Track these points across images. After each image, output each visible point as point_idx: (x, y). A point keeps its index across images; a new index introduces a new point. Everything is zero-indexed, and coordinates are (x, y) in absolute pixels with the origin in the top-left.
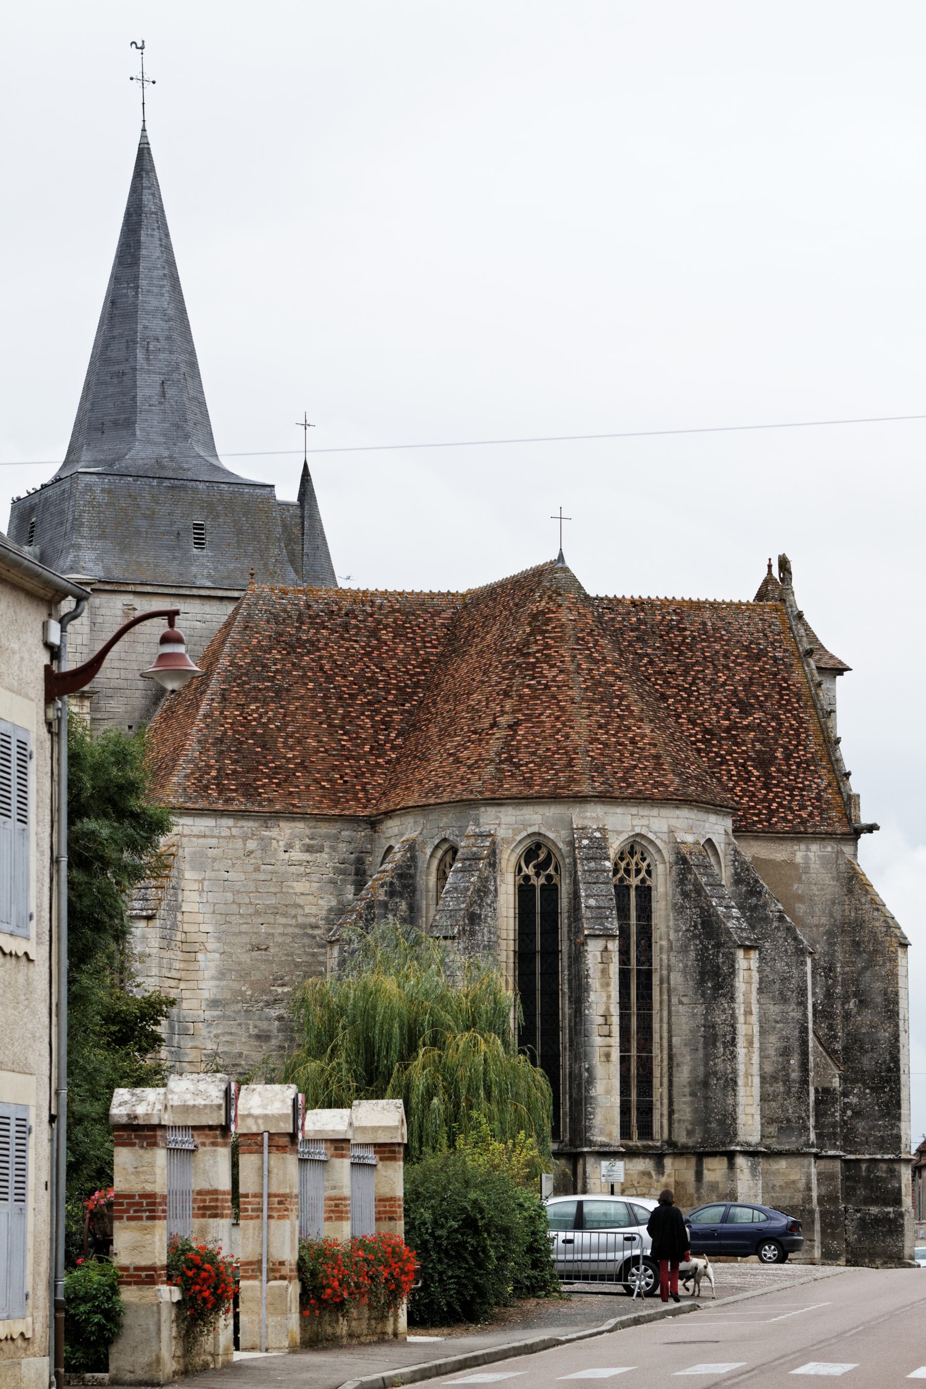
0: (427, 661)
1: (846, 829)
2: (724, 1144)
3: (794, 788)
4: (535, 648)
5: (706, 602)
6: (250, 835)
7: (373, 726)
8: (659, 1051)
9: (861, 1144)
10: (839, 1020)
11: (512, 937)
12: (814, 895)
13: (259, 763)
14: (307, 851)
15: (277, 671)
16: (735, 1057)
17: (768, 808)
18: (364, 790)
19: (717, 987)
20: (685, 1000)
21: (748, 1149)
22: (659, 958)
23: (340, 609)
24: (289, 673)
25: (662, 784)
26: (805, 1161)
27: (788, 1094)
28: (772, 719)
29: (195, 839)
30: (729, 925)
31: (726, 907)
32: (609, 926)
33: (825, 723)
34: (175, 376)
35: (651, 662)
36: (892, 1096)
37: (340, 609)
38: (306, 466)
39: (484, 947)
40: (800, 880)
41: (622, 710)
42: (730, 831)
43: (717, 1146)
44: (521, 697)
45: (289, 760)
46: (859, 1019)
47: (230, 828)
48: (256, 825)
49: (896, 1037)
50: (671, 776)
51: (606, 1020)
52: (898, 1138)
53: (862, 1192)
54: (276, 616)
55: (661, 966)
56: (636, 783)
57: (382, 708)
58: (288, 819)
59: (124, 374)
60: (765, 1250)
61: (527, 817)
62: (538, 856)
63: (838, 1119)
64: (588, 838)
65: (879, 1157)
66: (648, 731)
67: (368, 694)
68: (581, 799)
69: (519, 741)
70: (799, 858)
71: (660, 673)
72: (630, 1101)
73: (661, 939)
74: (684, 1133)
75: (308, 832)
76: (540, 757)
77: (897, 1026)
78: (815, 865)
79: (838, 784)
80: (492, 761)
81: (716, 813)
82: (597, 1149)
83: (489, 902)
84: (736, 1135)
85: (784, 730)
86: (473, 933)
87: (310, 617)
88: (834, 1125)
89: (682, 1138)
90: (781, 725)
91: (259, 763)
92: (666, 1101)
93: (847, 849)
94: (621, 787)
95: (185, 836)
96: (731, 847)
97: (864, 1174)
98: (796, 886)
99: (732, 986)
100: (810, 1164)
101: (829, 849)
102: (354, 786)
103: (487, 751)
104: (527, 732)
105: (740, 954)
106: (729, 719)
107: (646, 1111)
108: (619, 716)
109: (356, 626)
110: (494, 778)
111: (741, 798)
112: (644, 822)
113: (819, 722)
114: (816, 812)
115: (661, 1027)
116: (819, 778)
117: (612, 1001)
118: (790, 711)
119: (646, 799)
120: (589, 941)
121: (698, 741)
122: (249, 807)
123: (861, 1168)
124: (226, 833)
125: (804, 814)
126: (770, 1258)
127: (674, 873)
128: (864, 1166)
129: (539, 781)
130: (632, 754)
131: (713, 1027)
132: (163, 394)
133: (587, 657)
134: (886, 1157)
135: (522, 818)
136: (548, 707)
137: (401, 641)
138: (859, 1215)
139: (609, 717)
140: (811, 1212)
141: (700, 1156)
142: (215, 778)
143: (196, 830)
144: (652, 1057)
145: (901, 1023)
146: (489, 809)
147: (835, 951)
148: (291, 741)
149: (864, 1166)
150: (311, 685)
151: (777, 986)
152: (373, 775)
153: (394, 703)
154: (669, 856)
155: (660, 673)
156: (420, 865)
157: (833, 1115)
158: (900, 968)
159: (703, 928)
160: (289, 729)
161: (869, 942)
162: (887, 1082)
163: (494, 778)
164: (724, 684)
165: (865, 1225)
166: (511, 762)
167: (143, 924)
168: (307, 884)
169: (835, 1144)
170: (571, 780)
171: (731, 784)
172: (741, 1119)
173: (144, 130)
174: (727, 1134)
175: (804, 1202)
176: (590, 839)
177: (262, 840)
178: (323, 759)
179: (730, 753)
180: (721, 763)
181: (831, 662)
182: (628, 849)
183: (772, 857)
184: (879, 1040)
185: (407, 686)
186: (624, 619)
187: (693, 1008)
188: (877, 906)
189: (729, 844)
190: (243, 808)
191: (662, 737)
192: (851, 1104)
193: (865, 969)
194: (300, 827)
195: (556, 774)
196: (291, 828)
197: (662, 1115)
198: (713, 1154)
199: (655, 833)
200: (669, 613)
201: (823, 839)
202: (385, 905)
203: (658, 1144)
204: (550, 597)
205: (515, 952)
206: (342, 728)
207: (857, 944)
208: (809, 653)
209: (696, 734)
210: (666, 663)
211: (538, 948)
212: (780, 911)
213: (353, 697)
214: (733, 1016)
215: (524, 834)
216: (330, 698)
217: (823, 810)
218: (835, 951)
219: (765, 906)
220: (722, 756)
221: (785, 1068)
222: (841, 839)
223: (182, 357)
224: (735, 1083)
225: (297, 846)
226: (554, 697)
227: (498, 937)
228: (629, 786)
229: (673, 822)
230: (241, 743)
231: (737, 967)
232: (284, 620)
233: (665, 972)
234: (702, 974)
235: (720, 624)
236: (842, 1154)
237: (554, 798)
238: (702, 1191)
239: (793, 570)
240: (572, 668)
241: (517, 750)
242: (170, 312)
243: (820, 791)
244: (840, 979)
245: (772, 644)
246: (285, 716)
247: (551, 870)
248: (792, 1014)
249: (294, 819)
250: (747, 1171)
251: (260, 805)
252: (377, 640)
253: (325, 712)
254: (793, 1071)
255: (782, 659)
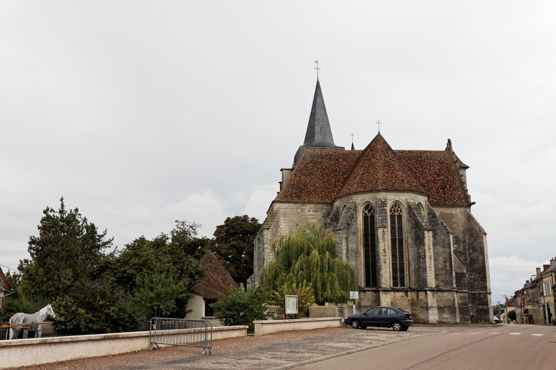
0: (351, 166)
1: (467, 204)
2: (424, 288)
3: (452, 194)
4: (370, 155)
5: (428, 151)
6: (298, 208)
7: (335, 181)
8: (405, 261)
9: (476, 289)
10: (468, 255)
11: (362, 230)
12: (459, 222)
13: (302, 190)
14: (314, 212)
15: (310, 169)
16: (426, 262)
17: (444, 199)
18: (331, 196)
19: (420, 242)
20: (412, 246)
21: (431, 289)
22: (405, 235)
23: (329, 154)
24: (314, 169)
25: (404, 187)
26: (452, 293)
27: (446, 274)
28: (446, 178)
29: (283, 209)
30: (423, 224)
31: (422, 219)
32: (385, 224)
33: (461, 178)
34: (323, 126)
35: (412, 165)
36: (484, 275)
37: (329, 154)
38: (353, 144)
39: (353, 233)
40: (454, 218)
41: (393, 168)
42: (427, 201)
43: (422, 288)
44: (365, 167)
45: (311, 189)
46: (473, 254)
47: (293, 206)
48: (300, 205)
49: (484, 259)
50: (407, 185)
51: (384, 251)
52: (486, 287)
53: (477, 302)
54: (312, 156)
55: (405, 237)
56: (396, 186)
57: (338, 177)
58: (309, 204)
59: (313, 127)
60: (395, 326)
61: (365, 197)
62: (369, 208)
63: (466, 281)
64: (381, 201)
65: (481, 292)
66: (400, 174)
67: (334, 174)
68: (379, 191)
69: (364, 178)
70: (454, 212)
71: (415, 167)
72: (397, 276)
73: (405, 230)
74: (413, 285)
75: (314, 207)
76: (369, 181)
77: (484, 256)
78: (459, 214)
79: (465, 193)
80: (356, 183)
81: (422, 195)
82: (383, 289)
83: (354, 220)
84: (427, 285)
85: (449, 180)
86: (348, 229)
87: (321, 156)
88: (465, 283)
89: (413, 286)
90: (448, 179)
91: (302, 190)
92: (408, 276)
93: (468, 210)
94: (391, 188)
95: (281, 208)
96: (427, 205)
97: (477, 297)
98: (453, 219)
99: (424, 241)
100: (454, 294)
101: (462, 210)
102: (328, 195)
103: (355, 181)
104: (366, 175)
105: (426, 232)
106: (434, 178)
107: (402, 278)
108: (392, 170)
109: (333, 158)
110: (356, 187)
111: (437, 197)
112: (399, 197)
113: (459, 178)
114: (458, 200)
115: (406, 254)
116: (459, 192)
117: (386, 246)
118: (451, 176)
119: (398, 190)
120: (379, 229)
121: (425, 183)
122: (298, 201)
123: (476, 295)
124: (292, 207)
125: (455, 201)
126: (397, 329)
127: (408, 211)
128: (477, 295)
129: (368, 187)
130: (395, 179)
131: (420, 254)
132: (321, 130)
133: (384, 156)
134: (483, 292)
135: (363, 197)
136: (372, 169)
137: (345, 161)
138: (476, 308)
139: (389, 170)
140: (455, 308)
141: (418, 291)
142: (290, 194)
143: (283, 207)
144: (404, 263)
145: (485, 255)
146: (355, 195)
147: (465, 236)
148: (312, 185)
149: (477, 295)
150: (319, 172)
151: (442, 243)
152: (333, 193)
153: (341, 176)
154: (406, 206)
155: (415, 167)
156: (340, 213)
157: (465, 280)
158: (484, 240)
159: (416, 225)
160: (312, 182)
161: (475, 233)
162: (482, 271)
163: (356, 187)
164: (433, 170)
165: (478, 311)
166: (361, 183)
167: (266, 230)
168: (315, 220)
169: (466, 288)
170: (377, 186)
171: (434, 194)
172: (428, 280)
173: (318, 78)
174: (424, 285)
175: (453, 305)
176: (381, 201)
177: (302, 209)
178: (320, 189)
179: (434, 186)
180: (431, 189)
181: (464, 166)
182: (394, 204)
183: (446, 212)
184: (479, 260)
185: (345, 171)
186: (405, 155)
187: (414, 249)
188: (477, 224)
189: (426, 204)
190: (296, 201)
191: (404, 175)
192: (472, 278)
193: (474, 241)
194: (312, 205)
195: (373, 185)
196: (310, 206)
197: (407, 280)
198: (421, 291)
199: (402, 200)
200: (418, 153)
201: (461, 207)
202: (330, 223)
203: (406, 288)
204: (375, 142)
205: (363, 234)
206: (326, 182)
207: (471, 234)
208: (456, 161)
209: (424, 182)
210: (416, 165)
211: (370, 233)
212: (441, 222)
213: (330, 174)
214: (425, 250)
215: (364, 202)
216: (324, 175)
217: (461, 200)
218: (465, 236)
219: (437, 220)
220: (431, 187)
221: (445, 266)
222: (465, 207)
223: (326, 123)
224: (426, 270)
225: (312, 210)
226: (374, 166)
227: (358, 230)
228: (393, 187)
229: (407, 197)
230: (298, 186)
231: (425, 236)
232: (314, 157)
233: (406, 239)
234: (416, 238)
235: (432, 156)
236: (468, 291)
237: (372, 191)
238: (419, 302)
239: (451, 142)
240: (379, 158)
241: (363, 180)
242: (323, 114)
243: (460, 195)
244: (467, 244)
245: (446, 160)
246: (311, 179)
247: (372, 211)
248: (446, 251)
249: (310, 204)
250: (431, 296)
251: (301, 200)
252: (338, 161)
253: (322, 178)
254: (448, 267)
255: (449, 164)
